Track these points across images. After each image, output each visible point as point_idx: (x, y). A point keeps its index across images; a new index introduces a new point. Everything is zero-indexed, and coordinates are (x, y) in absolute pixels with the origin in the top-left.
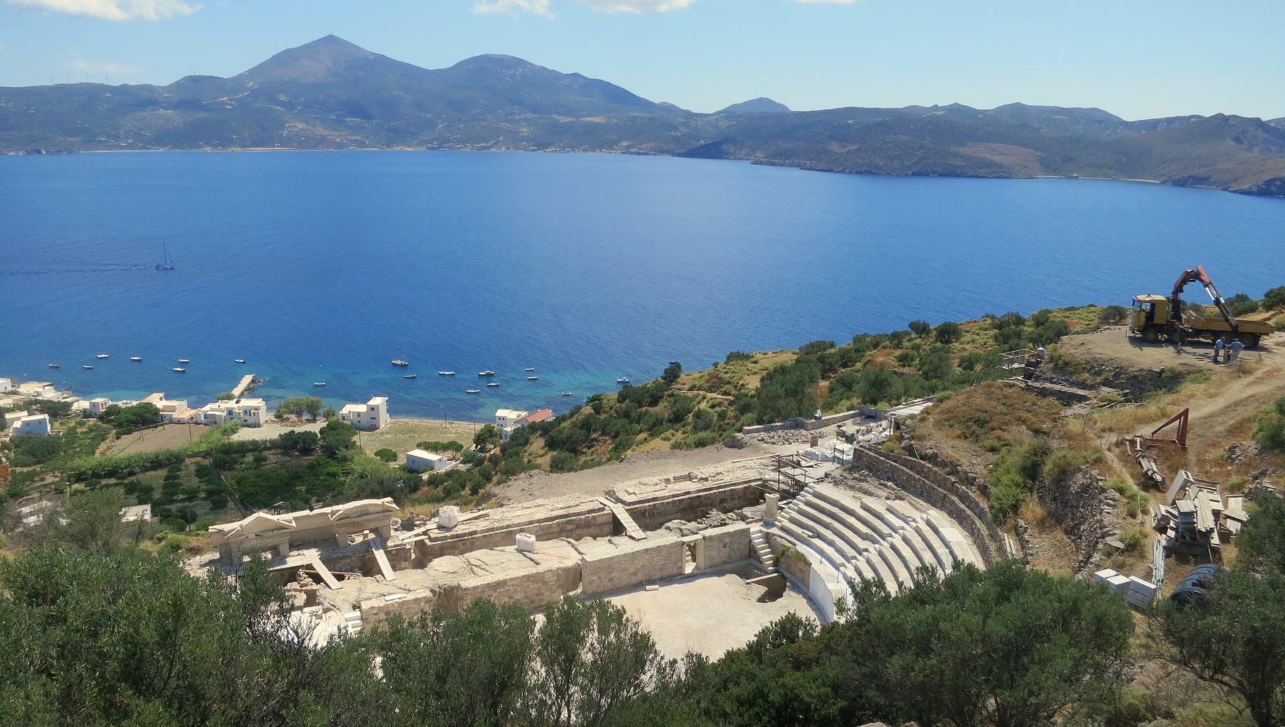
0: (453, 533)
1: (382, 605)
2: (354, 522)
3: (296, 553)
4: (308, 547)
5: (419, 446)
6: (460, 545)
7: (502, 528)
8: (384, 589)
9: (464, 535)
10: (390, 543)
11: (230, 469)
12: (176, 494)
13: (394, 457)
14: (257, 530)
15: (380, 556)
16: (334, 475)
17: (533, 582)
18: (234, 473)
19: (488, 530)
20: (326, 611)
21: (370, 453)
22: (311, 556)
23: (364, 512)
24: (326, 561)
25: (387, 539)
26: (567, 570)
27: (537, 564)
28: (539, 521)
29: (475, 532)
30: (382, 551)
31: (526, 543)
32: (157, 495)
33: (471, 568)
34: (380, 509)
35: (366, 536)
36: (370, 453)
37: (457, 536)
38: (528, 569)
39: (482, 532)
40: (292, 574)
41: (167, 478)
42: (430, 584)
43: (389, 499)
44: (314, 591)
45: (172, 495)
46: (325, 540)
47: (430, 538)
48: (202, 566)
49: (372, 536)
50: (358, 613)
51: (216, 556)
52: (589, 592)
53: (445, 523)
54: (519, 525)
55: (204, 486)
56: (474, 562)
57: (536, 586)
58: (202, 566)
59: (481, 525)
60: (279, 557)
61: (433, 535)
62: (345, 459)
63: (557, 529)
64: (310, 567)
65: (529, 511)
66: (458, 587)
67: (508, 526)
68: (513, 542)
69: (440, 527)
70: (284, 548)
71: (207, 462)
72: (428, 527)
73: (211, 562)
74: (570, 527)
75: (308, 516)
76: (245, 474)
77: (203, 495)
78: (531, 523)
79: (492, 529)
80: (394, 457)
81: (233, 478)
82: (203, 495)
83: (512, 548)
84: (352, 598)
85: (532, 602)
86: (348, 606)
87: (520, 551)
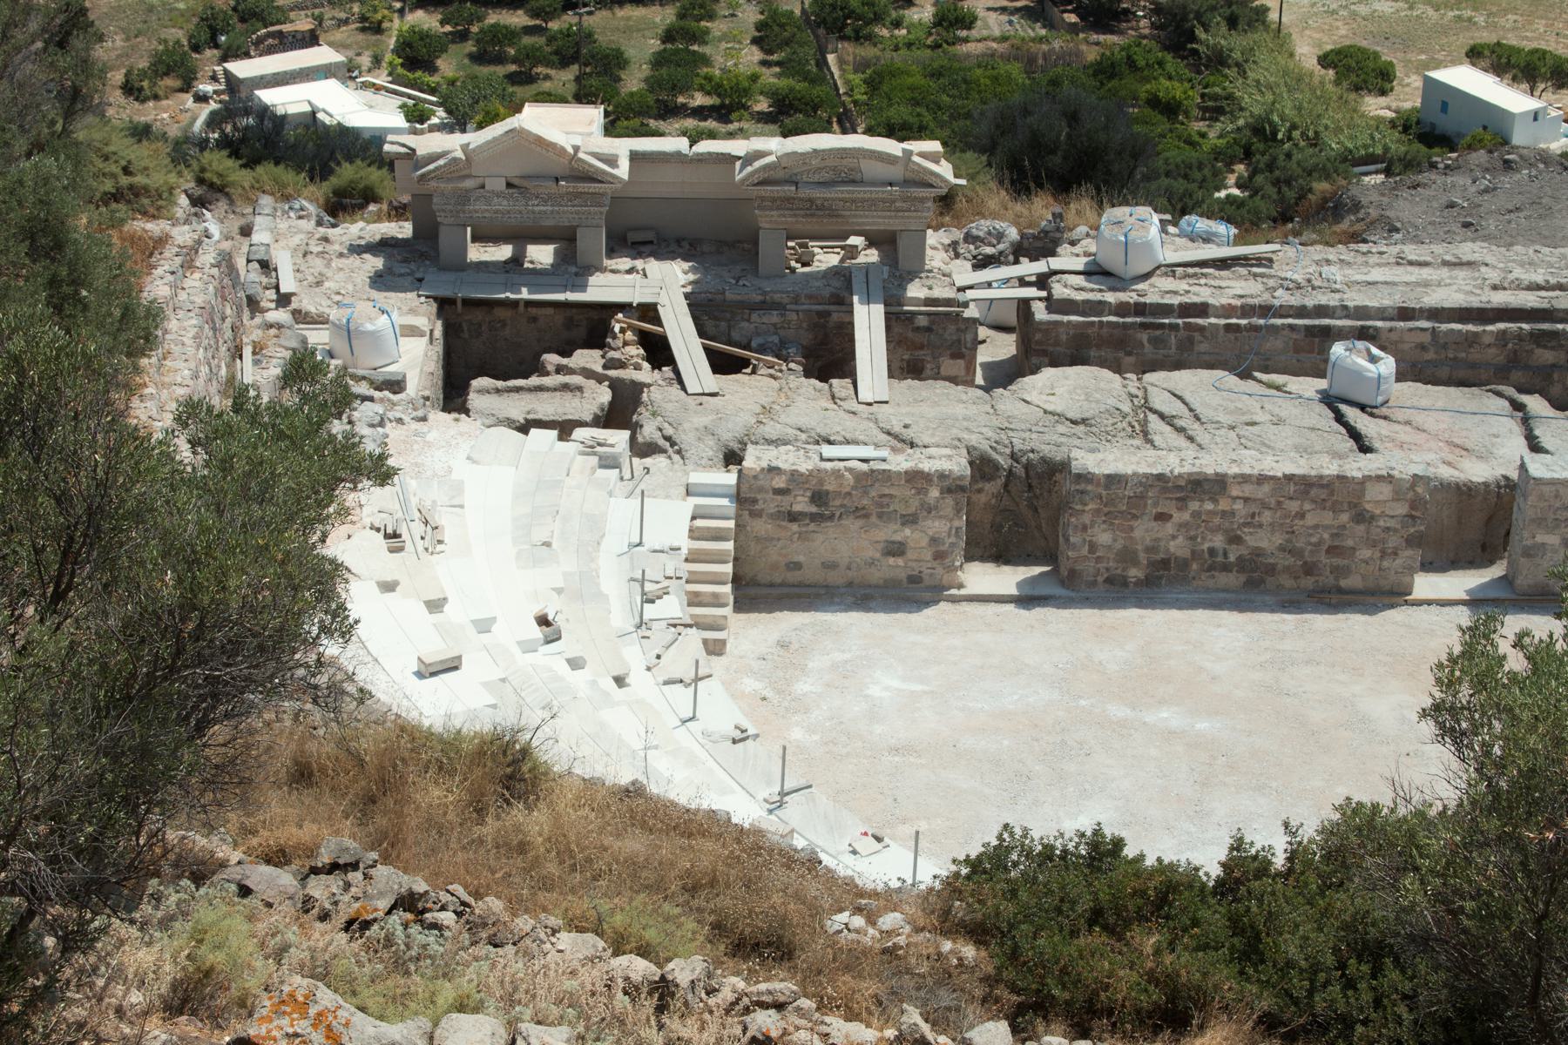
0: (1129, 297)
1: (804, 467)
2: (815, 200)
3: (624, 263)
4: (671, 256)
5: (1474, 55)
6: (1138, 338)
7: (1301, 312)
8: (837, 422)
9: (1165, 310)
10: (915, 291)
11: (857, 38)
12: (686, 89)
13: (1381, 79)
14: (513, 171)
15: (868, 325)
16: (1170, 109)
17: (1321, 504)
18: (867, 51)
19: (1247, 311)
20: (643, 450)
21: (1306, 53)
22: (666, 283)
23: (843, 171)
24: (702, 308)
25: (912, 275)
26: (1464, 492)
27: (1365, 448)
28: (1436, 314)
29: (1202, 309)
30: (878, 310)
31: (1358, 375)
32: (633, 82)
33: (1139, 424)
34: (896, 172)
35: (852, 252)
36: (1306, 53)
37: (1140, 309)
38: (1330, 458)
39: (1228, 311)
40: (592, 325)
41: (668, 36)
42: (981, 439)
43: (935, 146)
44: (638, 387)
45: (676, 88)
46: (717, 236)
47: (1053, 304)
48: (357, 250)
49: (871, 256)
50: (730, 478)
51: (404, 230)
52: (1522, 582)
53: (1112, 260)
54: (1361, 312)
55: (769, 77)
56: (1161, 401)
57: (1327, 518)
58: (357, 250)
59: (1236, 288)
60: (573, 267)
61: (1059, 291)
62: (1219, 60)
63: (1494, 355)
64: (649, 312)
65: (1415, 274)
66: (1064, 466)
67: (1321, 311)
68: (1318, 370)
69: (1096, 271)
70: (593, 239)
71: (963, 33)
72: (1055, 263)
73: (382, 246)
74: (1546, 356)
75: (677, 157)
76: (900, 58)
77: (762, 105)
78: (1405, 314)
79: (1266, 310)
80: (1381, 79)
81: (861, 66)
82: (762, 105)
83: (1310, 386)
84: (729, 433)
85: (1309, 569)
86: (710, 449)
87: (1330, 400)
